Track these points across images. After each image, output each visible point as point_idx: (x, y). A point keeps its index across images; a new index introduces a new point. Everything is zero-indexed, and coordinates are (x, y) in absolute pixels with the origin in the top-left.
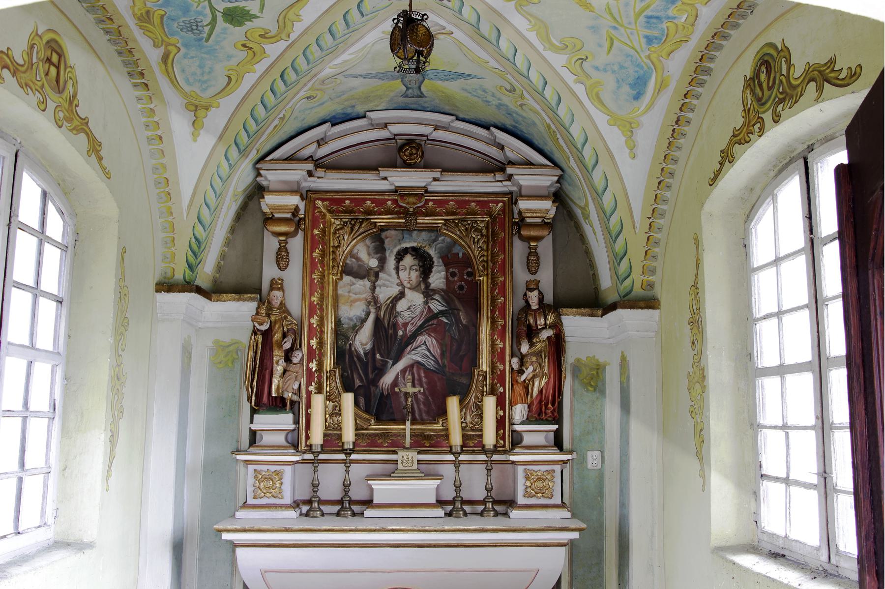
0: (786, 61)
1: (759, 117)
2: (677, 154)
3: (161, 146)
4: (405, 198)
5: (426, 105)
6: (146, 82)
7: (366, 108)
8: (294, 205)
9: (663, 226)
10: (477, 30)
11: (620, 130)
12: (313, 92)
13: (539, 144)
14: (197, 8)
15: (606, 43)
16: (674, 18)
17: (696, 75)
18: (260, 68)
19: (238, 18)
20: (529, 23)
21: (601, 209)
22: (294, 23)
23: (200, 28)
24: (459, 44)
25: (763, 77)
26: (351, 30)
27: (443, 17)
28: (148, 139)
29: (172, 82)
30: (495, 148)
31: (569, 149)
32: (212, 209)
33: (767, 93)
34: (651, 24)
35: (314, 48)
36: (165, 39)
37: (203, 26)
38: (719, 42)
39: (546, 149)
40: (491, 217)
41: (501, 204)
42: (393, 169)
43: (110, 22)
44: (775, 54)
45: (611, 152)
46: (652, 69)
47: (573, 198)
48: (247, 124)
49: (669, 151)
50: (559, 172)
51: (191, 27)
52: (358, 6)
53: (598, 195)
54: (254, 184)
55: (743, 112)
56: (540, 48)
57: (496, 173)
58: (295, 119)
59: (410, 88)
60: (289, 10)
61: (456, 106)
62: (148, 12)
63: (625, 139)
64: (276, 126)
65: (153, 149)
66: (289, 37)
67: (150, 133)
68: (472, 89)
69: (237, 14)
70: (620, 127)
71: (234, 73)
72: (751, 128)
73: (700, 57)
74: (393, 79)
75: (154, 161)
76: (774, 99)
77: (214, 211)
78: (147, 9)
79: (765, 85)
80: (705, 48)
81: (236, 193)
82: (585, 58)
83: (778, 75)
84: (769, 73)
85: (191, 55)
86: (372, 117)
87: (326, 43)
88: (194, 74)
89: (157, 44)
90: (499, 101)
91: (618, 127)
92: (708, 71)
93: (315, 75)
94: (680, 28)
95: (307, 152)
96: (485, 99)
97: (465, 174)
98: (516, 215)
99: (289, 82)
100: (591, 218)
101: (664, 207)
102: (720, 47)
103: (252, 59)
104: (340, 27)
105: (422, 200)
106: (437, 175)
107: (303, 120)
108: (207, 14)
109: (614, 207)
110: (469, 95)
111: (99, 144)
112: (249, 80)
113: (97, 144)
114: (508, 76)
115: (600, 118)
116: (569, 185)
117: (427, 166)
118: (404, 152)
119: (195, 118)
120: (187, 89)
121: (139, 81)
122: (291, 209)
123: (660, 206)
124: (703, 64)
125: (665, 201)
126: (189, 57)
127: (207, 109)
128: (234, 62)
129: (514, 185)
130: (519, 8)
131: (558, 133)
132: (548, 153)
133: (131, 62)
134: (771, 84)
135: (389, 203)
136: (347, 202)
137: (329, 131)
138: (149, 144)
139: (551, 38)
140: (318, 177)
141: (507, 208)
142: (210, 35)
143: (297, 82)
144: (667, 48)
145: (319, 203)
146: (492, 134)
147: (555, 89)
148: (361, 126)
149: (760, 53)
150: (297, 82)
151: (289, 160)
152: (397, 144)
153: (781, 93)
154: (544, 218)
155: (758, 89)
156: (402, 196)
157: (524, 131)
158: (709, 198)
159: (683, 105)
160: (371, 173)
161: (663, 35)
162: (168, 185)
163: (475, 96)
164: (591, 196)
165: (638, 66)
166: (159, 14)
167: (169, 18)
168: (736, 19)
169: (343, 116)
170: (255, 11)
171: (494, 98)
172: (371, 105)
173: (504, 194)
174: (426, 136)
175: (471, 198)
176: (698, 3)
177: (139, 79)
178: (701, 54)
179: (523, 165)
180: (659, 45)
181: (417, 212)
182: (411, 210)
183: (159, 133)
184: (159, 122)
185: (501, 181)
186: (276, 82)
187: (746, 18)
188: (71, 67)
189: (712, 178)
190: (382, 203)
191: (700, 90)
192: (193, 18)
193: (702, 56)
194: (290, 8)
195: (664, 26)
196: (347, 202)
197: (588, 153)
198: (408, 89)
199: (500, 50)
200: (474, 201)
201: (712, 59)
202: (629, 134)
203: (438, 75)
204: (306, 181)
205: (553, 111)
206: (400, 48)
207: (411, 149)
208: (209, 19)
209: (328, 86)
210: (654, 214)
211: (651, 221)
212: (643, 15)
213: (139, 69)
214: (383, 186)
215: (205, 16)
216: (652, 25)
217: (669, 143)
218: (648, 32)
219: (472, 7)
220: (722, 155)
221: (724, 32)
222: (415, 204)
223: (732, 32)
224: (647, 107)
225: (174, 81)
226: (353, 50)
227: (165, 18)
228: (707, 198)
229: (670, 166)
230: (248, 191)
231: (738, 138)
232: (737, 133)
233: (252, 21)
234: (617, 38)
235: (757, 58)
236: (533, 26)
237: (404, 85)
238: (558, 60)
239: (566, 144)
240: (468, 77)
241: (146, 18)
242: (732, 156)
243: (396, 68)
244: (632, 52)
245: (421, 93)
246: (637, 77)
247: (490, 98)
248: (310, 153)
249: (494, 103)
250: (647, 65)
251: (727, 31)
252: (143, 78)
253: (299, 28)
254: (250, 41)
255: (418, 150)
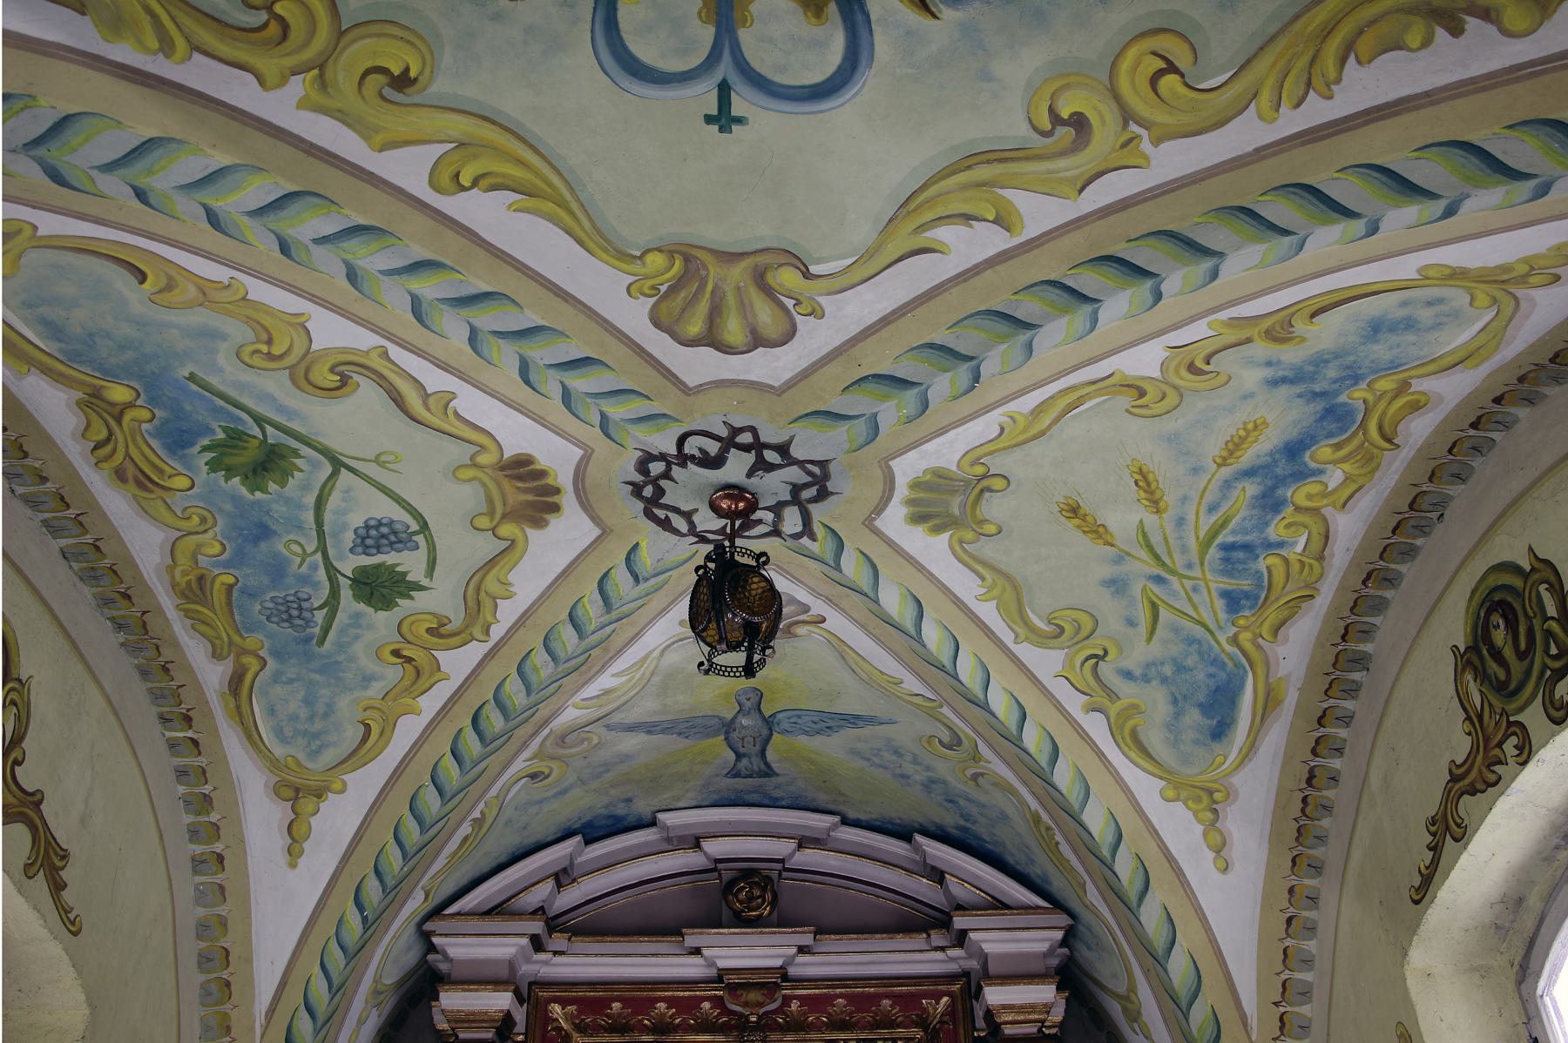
0: (1551, 589)
1: (1510, 724)
2: (1318, 852)
3: (219, 878)
4: (738, 992)
5: (777, 793)
6: (195, 736)
7: (655, 803)
8: (502, 1011)
9: (1310, 1019)
10: (872, 606)
11: (1189, 809)
12: (544, 763)
13: (1017, 863)
14: (299, 568)
15: (1143, 616)
16: (1281, 545)
17: (1338, 673)
18: (430, 703)
19: (384, 591)
20: (979, 581)
21: (1165, 991)
22: (498, 601)
23: (306, 614)
24: (839, 647)
25: (1499, 636)
26: (614, 615)
27: (801, 582)
28: (193, 860)
29: (249, 737)
30: (924, 880)
31: (1082, 863)
32: (321, 1019)
33: (1517, 668)
34: (1233, 564)
35: (540, 657)
36: (237, 639)
37: (312, 610)
38: (1380, 593)
39: (1034, 871)
40: (925, 1030)
41: (945, 999)
42: (713, 931)
43: (125, 603)
44: (1517, 582)
45: (1176, 862)
46: (1244, 668)
47: (1099, 978)
48: (403, 830)
49: (1300, 848)
50: (1064, 920)
51: (287, 611)
52: (628, 559)
53: (1156, 961)
54: (421, 971)
55: (1467, 722)
56: (1007, 637)
57: (932, 932)
58: (507, 824)
59: (744, 755)
60: (487, 573)
61: (841, 794)
62: (201, 579)
63: (1203, 827)
64: (466, 839)
65: (202, 884)
66: (487, 633)
67: (198, 849)
68: (872, 749)
69: (379, 581)
70: (1190, 803)
71: (375, 714)
72: (1497, 752)
73: (1343, 631)
74: (708, 736)
75: (203, 910)
76: (1542, 673)
77: (325, 1023)
78: (199, 572)
79: (1508, 652)
80: (1351, 610)
81: (380, 987)
82: (1101, 653)
83: (1537, 623)
84: (1512, 626)
85: (289, 675)
86: (669, 823)
87: (565, 645)
88: (294, 718)
89: (219, 651)
90: (929, 774)
91: (1185, 804)
92: (1361, 661)
93: (546, 722)
94: (1296, 567)
95: (534, 898)
96: (898, 771)
97: (864, 936)
98: (980, 1023)
99: (489, 736)
100: (1145, 1017)
101: (1307, 976)
102: (1380, 606)
103: (413, 684)
104: (592, 610)
105: (776, 996)
106: (807, 939)
107: (525, 828)
108: (319, 582)
109: (1195, 985)
110: (865, 763)
111: (62, 853)
112: (408, 730)
113: (56, 854)
114: (945, 710)
115: (1145, 786)
116: (1089, 948)
117: (785, 922)
118: (736, 895)
119: (293, 816)
120: (279, 751)
121: (182, 734)
122: (494, 1021)
123: (1298, 976)
124: (1351, 646)
125: (1307, 962)
126: (284, 679)
127: (319, 796)
128: (375, 690)
129: (970, 956)
130: (957, 547)
131: (1057, 832)
132: (1038, 881)
133: (166, 692)
134: (1523, 646)
135: (706, 1005)
136: (616, 1006)
137: (580, 855)
138: (195, 872)
139: (1029, 612)
140: (556, 953)
141: (960, 1007)
142: (326, 630)
143: (508, 734)
144: (1272, 615)
145: (556, 1009)
146: (918, 849)
147: (1045, 729)
148: (646, 844)
149: (1479, 592)
150: (508, 734)
151: (497, 914)
152: (721, 881)
153: (1555, 658)
154: (1043, 1022)
155: (1492, 666)
156: (733, 988)
157: (985, 837)
158: (1419, 932)
159: (1318, 741)
160: (668, 941)
161: (1260, 586)
162: (228, 965)
163: (881, 766)
164: (1142, 967)
165: (1215, 661)
166: (223, 584)
167: (243, 591)
168: (1408, 537)
169: (610, 822)
170: (416, 573)
171: (918, 768)
172: (665, 796)
173: (950, 978)
174: (782, 861)
175: (881, 990)
176: (1326, 506)
177: (181, 730)
178: (1343, 624)
179: (987, 910)
180: (1253, 612)
181: (766, 1024)
182: (754, 1019)
183: (218, 847)
184: (219, 823)
185: (942, 949)
186: (463, 734)
187: (1430, 533)
188: (19, 680)
189: (1417, 885)
190: (687, 1006)
191: (1349, 705)
192: (292, 592)
193: (1346, 628)
194: (487, 567)
195: (1262, 565)
196: (616, 1006)
197: (1124, 867)
198: (739, 756)
199: (924, 646)
200: (887, 996)
201: (1367, 633)
202: (1209, 815)
203: (799, 721)
204: (528, 961)
205: (1041, 778)
206: (710, 621)
207: (751, 888)
208: (325, 592)
209: (573, 751)
210: (1286, 994)
211: (1282, 1009)
212: (1215, 544)
213: (183, 708)
214: (691, 968)
215: (316, 585)
216: (1236, 566)
217: (1299, 830)
218: (1229, 584)
219: (861, 552)
220: (1433, 829)
221: (1388, 569)
222: (761, 1005)
223: (1403, 568)
224: (1243, 752)
225: (251, 736)
226: (621, 664)
227: (235, 594)
228: (1413, 935)
229: (1307, 881)
230: (408, 985)
231: (1467, 781)
232: (1460, 771)
233: (412, 598)
234: (1167, 604)
235: (1474, 603)
236: (990, 589)
237: (731, 748)
238: (1046, 662)
239: (1075, 851)
240: (861, 723)
241: (198, 592)
242: (1458, 826)
243: (701, 664)
244: (1198, 631)
245: (767, 764)
246: (1214, 688)
247: (909, 768)
248: (539, 902)
249: (918, 777)
250: (1231, 659)
251: (1393, 566)
252: (190, 727)
253: (508, 613)
254: (409, 642)
255: (764, 889)
